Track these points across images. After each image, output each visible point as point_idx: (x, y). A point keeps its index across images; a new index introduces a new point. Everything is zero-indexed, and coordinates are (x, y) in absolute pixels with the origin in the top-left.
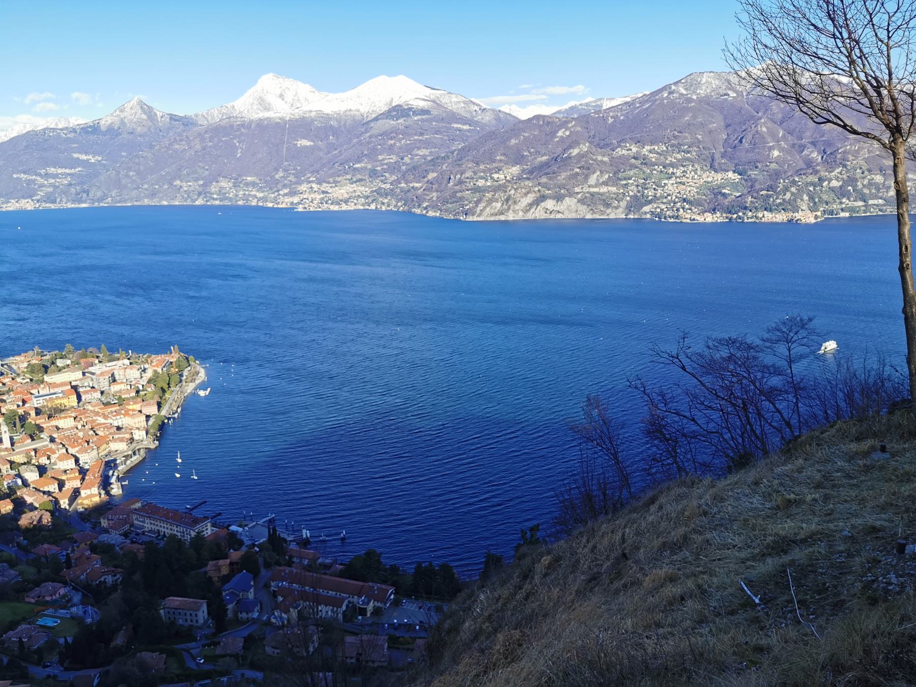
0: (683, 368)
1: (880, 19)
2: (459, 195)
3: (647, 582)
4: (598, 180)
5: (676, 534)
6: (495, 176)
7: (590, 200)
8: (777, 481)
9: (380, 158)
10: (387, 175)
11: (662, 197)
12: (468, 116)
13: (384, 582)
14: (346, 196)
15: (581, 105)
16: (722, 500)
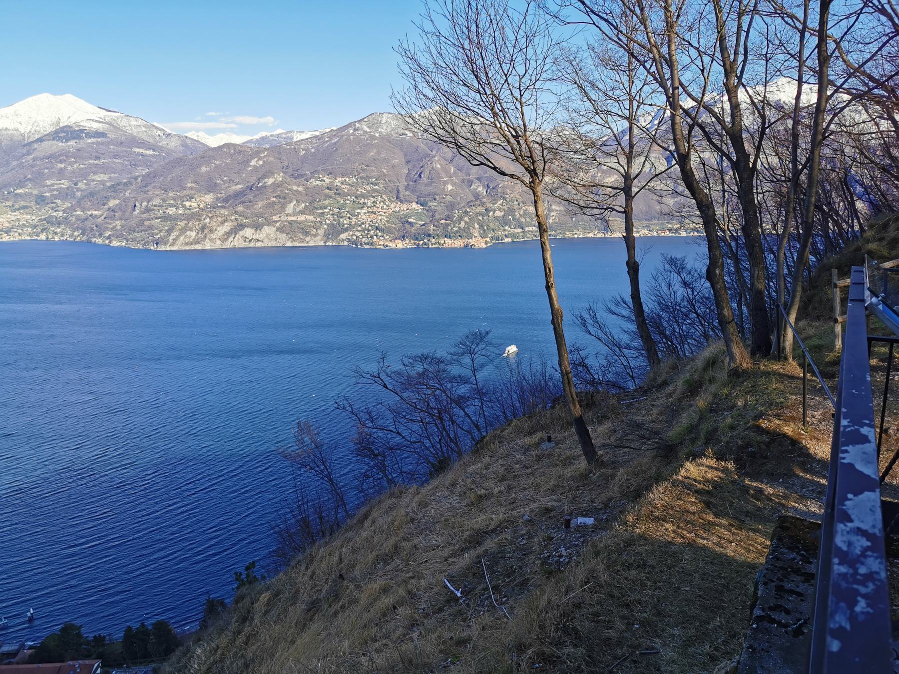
0: (385, 386)
1: (513, 80)
2: (147, 223)
3: (364, 599)
4: (295, 209)
5: (388, 546)
6: (188, 204)
7: (288, 229)
8: (470, 480)
9: (48, 182)
10: (59, 202)
11: (357, 225)
12: (151, 141)
13: (87, 657)
14: (7, 225)
15: (271, 136)
16: (427, 505)
